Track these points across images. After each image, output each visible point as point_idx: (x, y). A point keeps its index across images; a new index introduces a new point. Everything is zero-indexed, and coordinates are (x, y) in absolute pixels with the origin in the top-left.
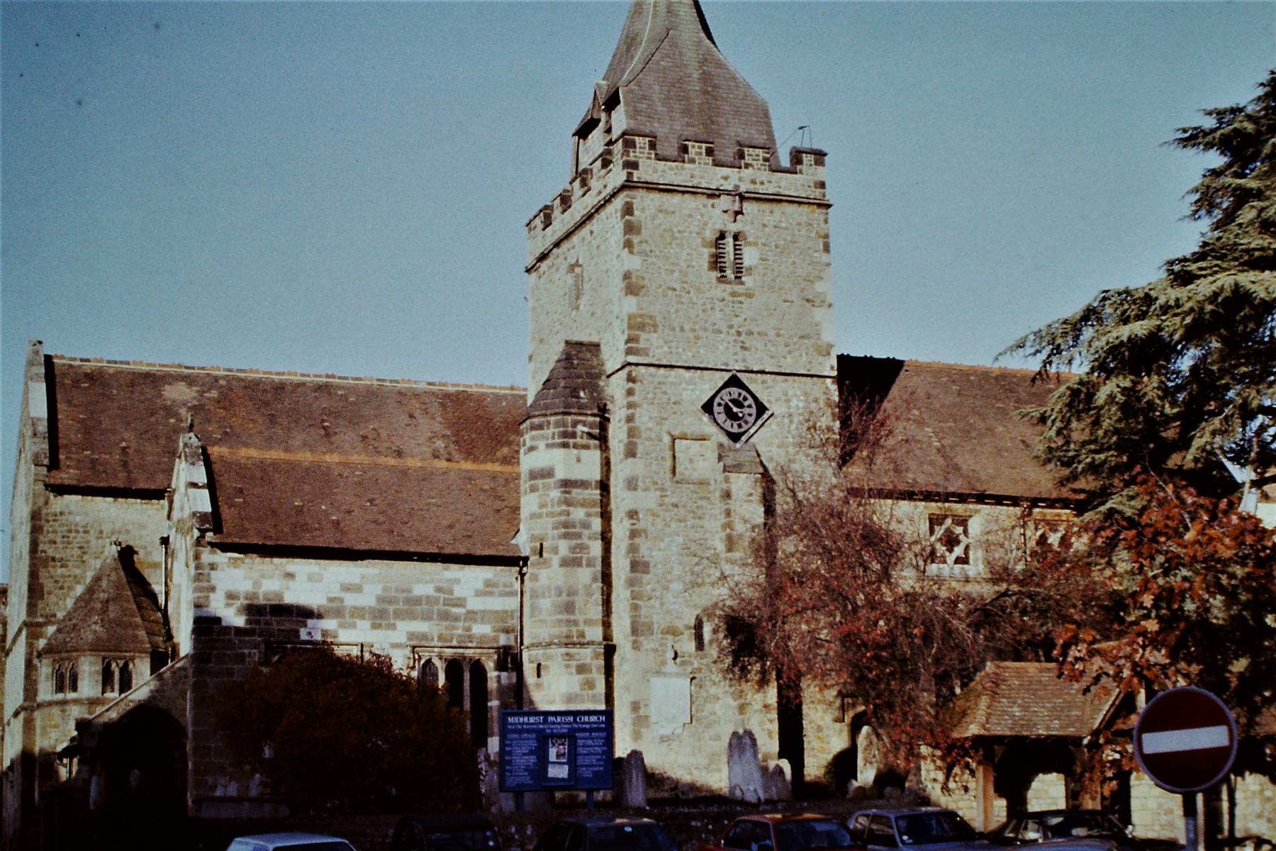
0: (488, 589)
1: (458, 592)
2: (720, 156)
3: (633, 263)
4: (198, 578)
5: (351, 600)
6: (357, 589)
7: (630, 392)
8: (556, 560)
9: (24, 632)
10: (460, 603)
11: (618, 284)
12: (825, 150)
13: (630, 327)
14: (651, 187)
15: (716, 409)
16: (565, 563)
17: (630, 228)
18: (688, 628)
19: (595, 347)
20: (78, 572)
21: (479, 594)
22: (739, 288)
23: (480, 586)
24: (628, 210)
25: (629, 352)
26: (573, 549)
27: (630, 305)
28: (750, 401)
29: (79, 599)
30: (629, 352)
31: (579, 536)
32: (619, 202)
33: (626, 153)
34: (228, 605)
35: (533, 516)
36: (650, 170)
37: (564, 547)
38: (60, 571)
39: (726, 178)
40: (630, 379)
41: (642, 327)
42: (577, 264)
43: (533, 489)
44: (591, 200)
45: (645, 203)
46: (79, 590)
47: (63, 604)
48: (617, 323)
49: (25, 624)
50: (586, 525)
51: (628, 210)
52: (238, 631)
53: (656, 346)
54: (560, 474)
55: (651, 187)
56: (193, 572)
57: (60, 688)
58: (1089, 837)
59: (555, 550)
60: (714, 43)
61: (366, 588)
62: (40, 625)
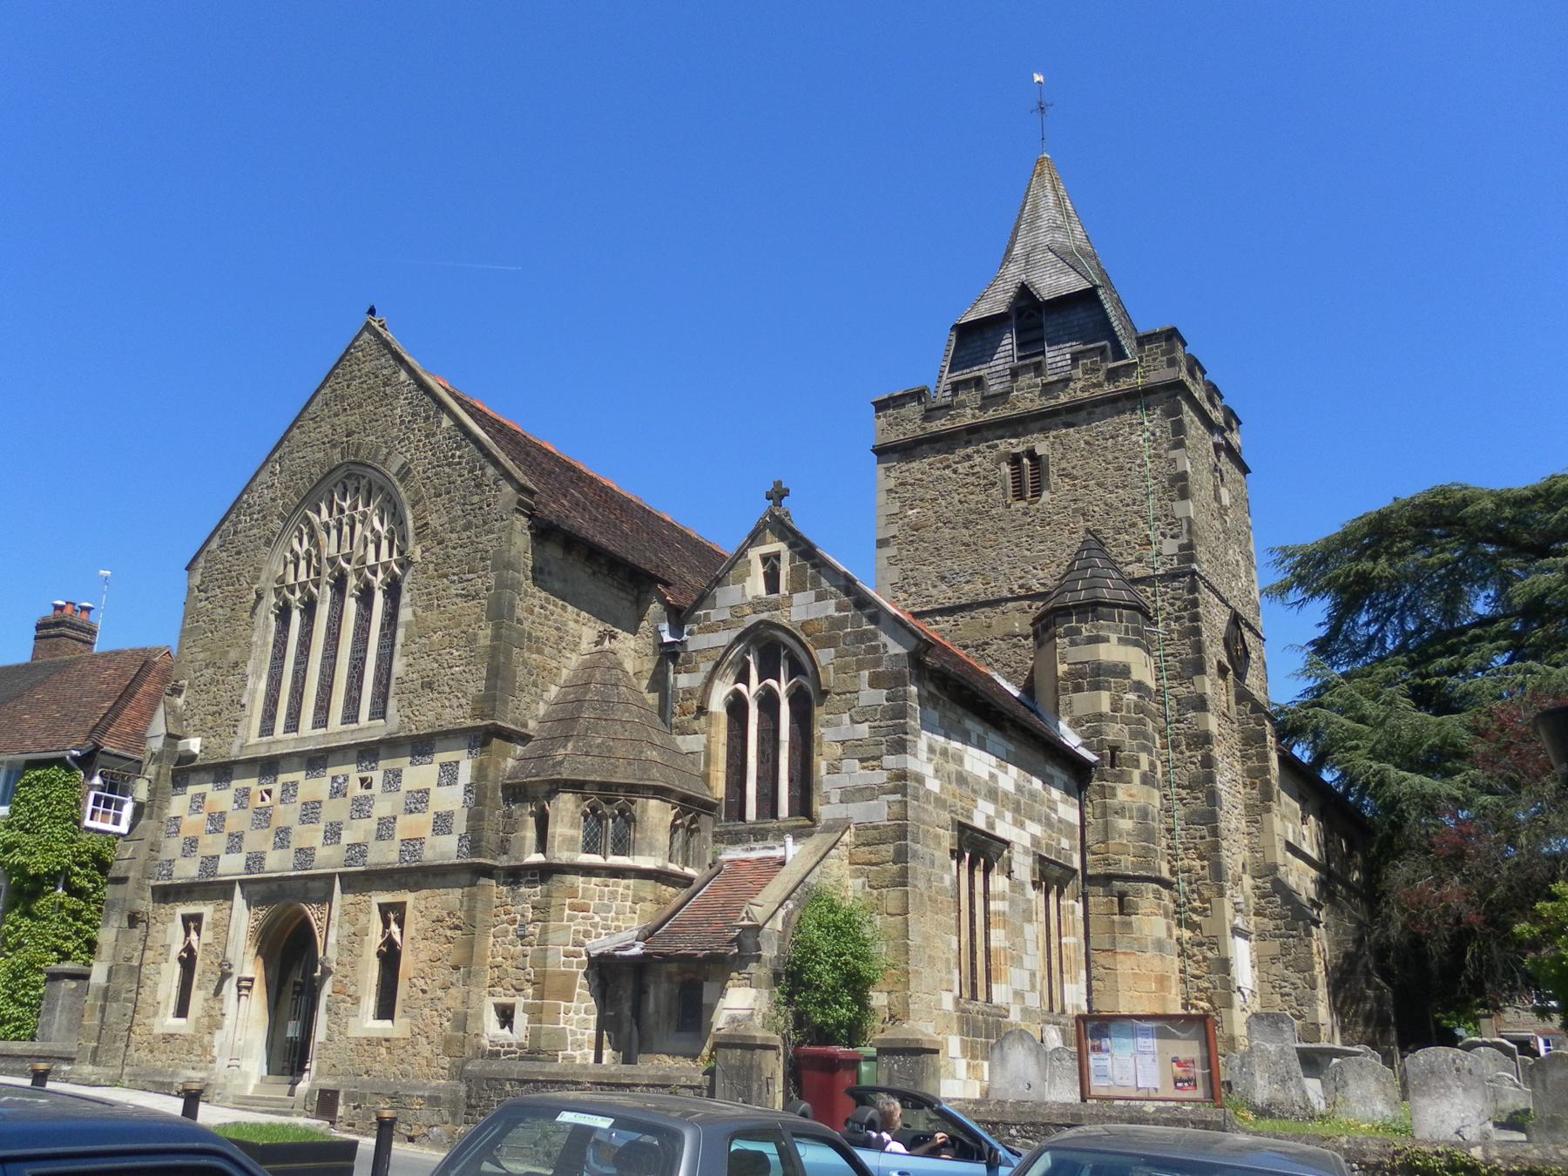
8: (1136, 775)
57: (589, 848)
59: (1136, 763)
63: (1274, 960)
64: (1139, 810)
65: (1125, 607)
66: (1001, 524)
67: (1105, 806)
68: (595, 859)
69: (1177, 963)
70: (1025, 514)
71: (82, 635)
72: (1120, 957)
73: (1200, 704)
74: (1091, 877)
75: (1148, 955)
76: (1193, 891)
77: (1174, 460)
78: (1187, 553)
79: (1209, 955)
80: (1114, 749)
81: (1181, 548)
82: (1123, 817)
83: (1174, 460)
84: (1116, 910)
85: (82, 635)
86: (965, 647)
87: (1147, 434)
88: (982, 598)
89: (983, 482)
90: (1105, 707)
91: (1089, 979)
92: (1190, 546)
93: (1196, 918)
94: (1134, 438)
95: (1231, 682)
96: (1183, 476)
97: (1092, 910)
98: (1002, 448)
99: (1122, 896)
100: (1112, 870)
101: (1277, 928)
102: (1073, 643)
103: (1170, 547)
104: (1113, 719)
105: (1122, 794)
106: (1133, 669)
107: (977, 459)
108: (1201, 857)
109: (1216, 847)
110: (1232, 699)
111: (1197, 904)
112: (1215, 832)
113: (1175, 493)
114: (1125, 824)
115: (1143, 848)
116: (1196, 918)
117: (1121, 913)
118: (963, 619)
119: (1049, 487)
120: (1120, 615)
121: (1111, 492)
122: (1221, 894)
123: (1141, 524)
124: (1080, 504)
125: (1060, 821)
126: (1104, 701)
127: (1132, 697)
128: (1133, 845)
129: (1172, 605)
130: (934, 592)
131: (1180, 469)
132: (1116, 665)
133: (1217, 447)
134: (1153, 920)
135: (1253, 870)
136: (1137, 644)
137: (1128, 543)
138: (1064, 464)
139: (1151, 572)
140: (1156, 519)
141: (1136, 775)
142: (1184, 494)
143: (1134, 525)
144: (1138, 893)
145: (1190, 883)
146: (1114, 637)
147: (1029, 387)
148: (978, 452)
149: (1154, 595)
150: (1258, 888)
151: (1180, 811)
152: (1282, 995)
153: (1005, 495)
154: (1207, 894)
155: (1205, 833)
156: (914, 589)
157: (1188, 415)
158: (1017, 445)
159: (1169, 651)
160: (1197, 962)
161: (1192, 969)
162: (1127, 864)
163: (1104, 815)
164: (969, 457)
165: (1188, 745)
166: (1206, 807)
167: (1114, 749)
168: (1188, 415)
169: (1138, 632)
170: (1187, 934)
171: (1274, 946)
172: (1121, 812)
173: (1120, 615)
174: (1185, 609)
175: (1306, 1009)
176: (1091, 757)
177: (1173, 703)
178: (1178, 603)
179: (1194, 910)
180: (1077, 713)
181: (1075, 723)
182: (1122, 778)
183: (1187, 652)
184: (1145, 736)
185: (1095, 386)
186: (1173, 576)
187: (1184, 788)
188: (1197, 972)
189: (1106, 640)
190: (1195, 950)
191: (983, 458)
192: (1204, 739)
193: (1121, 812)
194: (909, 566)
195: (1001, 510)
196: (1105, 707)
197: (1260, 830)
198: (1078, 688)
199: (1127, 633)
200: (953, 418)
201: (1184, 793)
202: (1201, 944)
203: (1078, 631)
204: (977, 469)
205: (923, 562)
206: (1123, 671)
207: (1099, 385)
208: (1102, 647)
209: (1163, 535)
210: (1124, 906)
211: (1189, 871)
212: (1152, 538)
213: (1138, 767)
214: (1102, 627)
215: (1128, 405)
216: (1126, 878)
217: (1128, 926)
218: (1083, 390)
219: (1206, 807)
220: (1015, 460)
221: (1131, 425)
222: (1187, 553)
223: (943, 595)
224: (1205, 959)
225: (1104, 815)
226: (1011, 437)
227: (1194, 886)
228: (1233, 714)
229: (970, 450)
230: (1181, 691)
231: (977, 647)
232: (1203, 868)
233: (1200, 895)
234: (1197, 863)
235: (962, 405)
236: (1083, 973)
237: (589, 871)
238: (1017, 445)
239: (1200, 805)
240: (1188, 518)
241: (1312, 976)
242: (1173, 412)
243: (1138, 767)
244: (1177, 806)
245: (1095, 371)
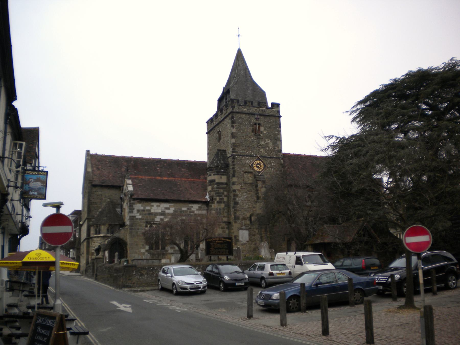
0: (200, 209)
1: (193, 209)
2: (254, 105)
3: (234, 130)
4: (130, 206)
5: (167, 211)
6: (168, 209)
7: (233, 162)
8: (216, 202)
9: (86, 221)
10: (193, 212)
11: (230, 135)
12: (280, 103)
13: (233, 146)
14: (238, 113)
15: (254, 166)
16: (218, 202)
17: (233, 122)
18: (248, 218)
19: (224, 151)
20: (100, 206)
21: (197, 210)
22: (259, 137)
23: (197, 208)
24: (232, 118)
25: (233, 152)
26: (220, 199)
27: (233, 141)
28: (262, 164)
29: (100, 212)
30: (233, 152)
31: (221, 196)
32: (230, 116)
33: (232, 104)
34: (137, 213)
35: (210, 191)
36: (236, 109)
37: (218, 199)
38: (96, 205)
39: (256, 110)
40: (234, 158)
41: (236, 146)
42: (220, 131)
43: (210, 185)
44: (223, 116)
45: (236, 117)
46: (100, 210)
47: (96, 214)
48: (230, 145)
49: (87, 219)
50: (223, 193)
51: (232, 118)
52: (140, 219)
53: (240, 150)
54: (217, 181)
55: (238, 113)
56: (129, 205)
57: (96, 234)
58: (363, 225)
59: (216, 199)
60: (3, 168)
61: (171, 208)
62: (90, 219)
68: (96, 236)
71: (98, 232)
85: (98, 232)
104: (212, 191)
105: (406, 178)
127: (215, 186)
141: (216, 202)
146: (212, 174)
172: (213, 210)
182: (213, 203)
193: (213, 210)
237: (95, 237)
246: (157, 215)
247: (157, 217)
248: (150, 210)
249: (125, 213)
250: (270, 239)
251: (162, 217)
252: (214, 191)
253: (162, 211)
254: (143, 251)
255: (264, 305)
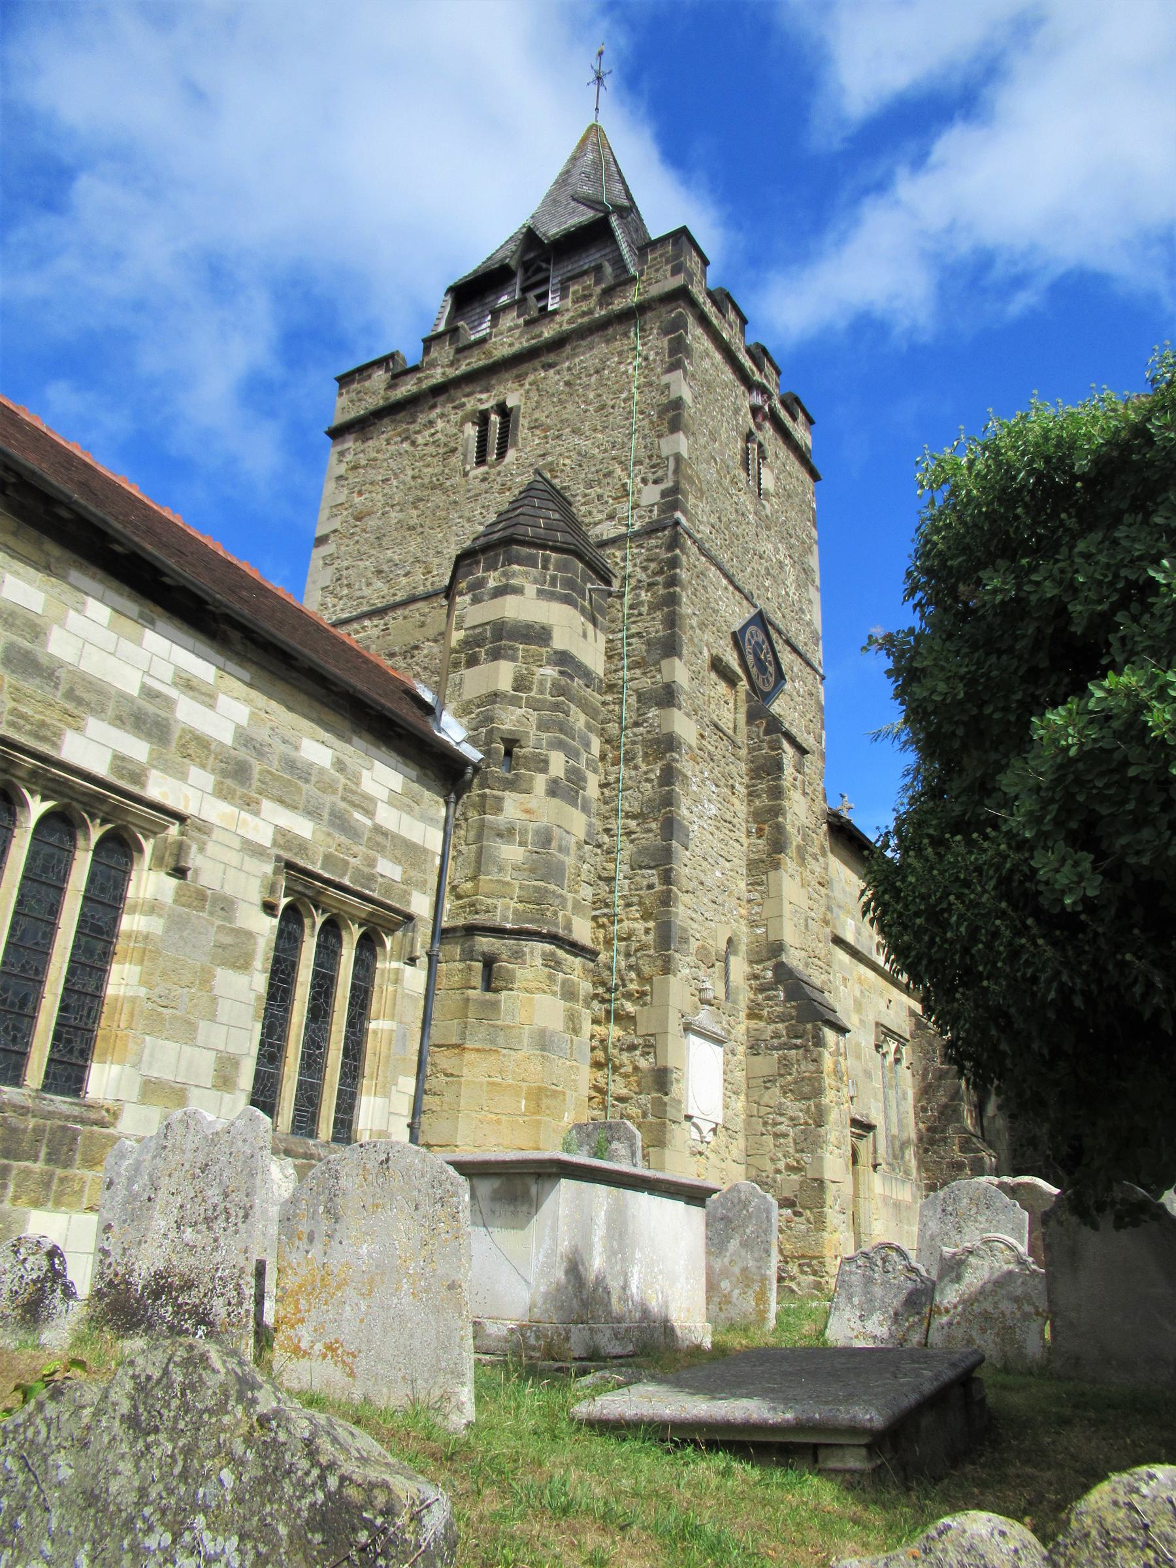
6: (208, 698)
8: (540, 782)
59: (542, 765)
63: (769, 1081)
64: (537, 832)
65: (555, 549)
66: (453, 497)
67: (482, 826)
69: (585, 1076)
70: (484, 480)
72: (469, 1056)
73: (667, 696)
74: (445, 931)
75: (519, 1055)
76: (630, 967)
77: (667, 386)
78: (672, 500)
79: (643, 1063)
80: (511, 743)
81: (664, 494)
82: (510, 842)
83: (667, 386)
84: (477, 980)
86: (392, 655)
87: (639, 360)
88: (421, 590)
89: (441, 451)
90: (505, 684)
91: (420, 1092)
92: (675, 490)
93: (630, 1007)
94: (622, 368)
95: (742, 696)
96: (677, 404)
97: (442, 982)
98: (469, 407)
99: (489, 962)
100: (481, 919)
101: (776, 1035)
102: (476, 600)
103: (651, 495)
104: (515, 702)
105: (513, 807)
106: (556, 635)
107: (440, 424)
108: (646, 917)
109: (666, 900)
110: (742, 717)
111: (633, 987)
112: (667, 878)
113: (664, 427)
114: (512, 853)
115: (537, 889)
116: (630, 1007)
117: (488, 987)
118: (395, 620)
119: (515, 444)
120: (546, 560)
121: (587, 438)
122: (667, 968)
123: (619, 471)
124: (550, 459)
125: (378, 830)
126: (503, 675)
127: (550, 672)
128: (517, 884)
129: (645, 569)
130: (367, 591)
131: (673, 396)
132: (529, 626)
133: (755, 410)
134: (537, 999)
135: (750, 952)
136: (567, 600)
137: (600, 497)
138: (537, 415)
139: (623, 530)
140: (638, 462)
141: (540, 782)
142: (675, 426)
143: (608, 474)
144: (517, 956)
145: (628, 955)
146: (531, 589)
147: (510, 329)
148: (442, 416)
149: (624, 559)
150: (756, 977)
151: (626, 851)
152: (776, 1136)
153: (464, 462)
154: (647, 970)
155: (655, 880)
156: (345, 591)
157: (696, 336)
158: (486, 401)
159: (634, 629)
160: (626, 1076)
161: (618, 1087)
162: (505, 910)
163: (479, 838)
164: (431, 423)
165: (646, 755)
166: (659, 842)
167: (511, 743)
168: (696, 336)
169: (569, 584)
170: (614, 1031)
171: (767, 1064)
172: (507, 834)
173: (546, 560)
174: (661, 572)
175: (807, 1158)
176: (473, 754)
177: (633, 700)
178: (653, 566)
179: (628, 996)
180: (467, 696)
181: (464, 711)
183: (656, 627)
184: (563, 728)
185: (584, 314)
186: (651, 530)
187: (634, 817)
188: (624, 1092)
189: (518, 591)
190: (625, 1057)
191: (452, 426)
192: (667, 744)
193: (507, 834)
194: (345, 564)
195: (458, 479)
196: (505, 684)
197: (765, 894)
198: (472, 661)
199: (553, 583)
200: (420, 380)
201: (632, 824)
202: (632, 1048)
203: (481, 583)
204: (439, 435)
205: (361, 556)
206: (539, 635)
207: (591, 312)
208: (510, 600)
209: (644, 481)
210: (492, 975)
211: (627, 939)
212: (630, 488)
213: (544, 770)
214: (514, 575)
215: (620, 329)
216: (499, 932)
217: (494, 1006)
218: (570, 322)
219: (659, 842)
220: (483, 420)
221: (620, 354)
222: (672, 500)
223: (377, 593)
224: (636, 1069)
225: (479, 838)
226: (481, 392)
227: (632, 960)
228: (741, 738)
229: (433, 414)
230: (645, 683)
231: (404, 655)
232: (647, 931)
233: (639, 974)
234: (640, 926)
235: (433, 364)
236: (408, 1084)
238: (486, 401)
239: (650, 836)
240: (678, 458)
241: (818, 1106)
242: (678, 325)
243: (544, 770)
244: (622, 842)
245: (585, 297)
246: (99, 711)
247: (95, 726)
248: (36, 631)
249: (130, 540)
250: (422, 1472)
251: (138, 749)
252: (535, 705)
253: (149, 693)
254: (1042, 732)
255: (976, 1374)
